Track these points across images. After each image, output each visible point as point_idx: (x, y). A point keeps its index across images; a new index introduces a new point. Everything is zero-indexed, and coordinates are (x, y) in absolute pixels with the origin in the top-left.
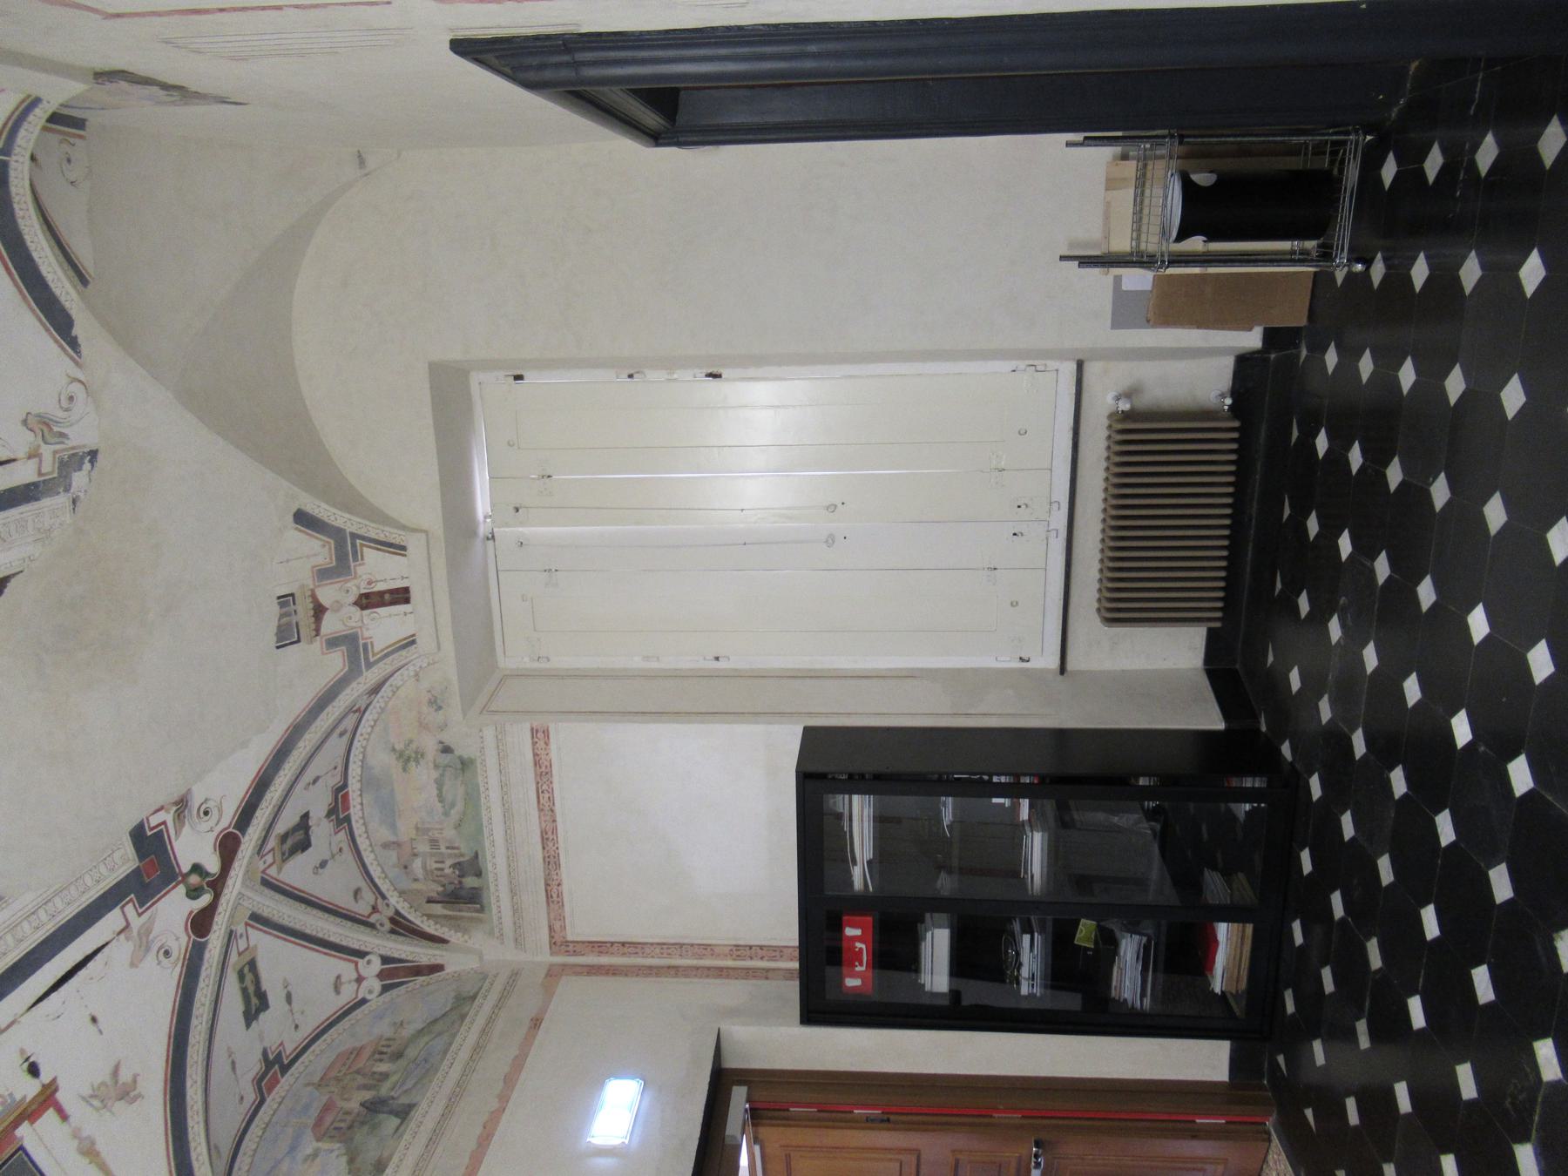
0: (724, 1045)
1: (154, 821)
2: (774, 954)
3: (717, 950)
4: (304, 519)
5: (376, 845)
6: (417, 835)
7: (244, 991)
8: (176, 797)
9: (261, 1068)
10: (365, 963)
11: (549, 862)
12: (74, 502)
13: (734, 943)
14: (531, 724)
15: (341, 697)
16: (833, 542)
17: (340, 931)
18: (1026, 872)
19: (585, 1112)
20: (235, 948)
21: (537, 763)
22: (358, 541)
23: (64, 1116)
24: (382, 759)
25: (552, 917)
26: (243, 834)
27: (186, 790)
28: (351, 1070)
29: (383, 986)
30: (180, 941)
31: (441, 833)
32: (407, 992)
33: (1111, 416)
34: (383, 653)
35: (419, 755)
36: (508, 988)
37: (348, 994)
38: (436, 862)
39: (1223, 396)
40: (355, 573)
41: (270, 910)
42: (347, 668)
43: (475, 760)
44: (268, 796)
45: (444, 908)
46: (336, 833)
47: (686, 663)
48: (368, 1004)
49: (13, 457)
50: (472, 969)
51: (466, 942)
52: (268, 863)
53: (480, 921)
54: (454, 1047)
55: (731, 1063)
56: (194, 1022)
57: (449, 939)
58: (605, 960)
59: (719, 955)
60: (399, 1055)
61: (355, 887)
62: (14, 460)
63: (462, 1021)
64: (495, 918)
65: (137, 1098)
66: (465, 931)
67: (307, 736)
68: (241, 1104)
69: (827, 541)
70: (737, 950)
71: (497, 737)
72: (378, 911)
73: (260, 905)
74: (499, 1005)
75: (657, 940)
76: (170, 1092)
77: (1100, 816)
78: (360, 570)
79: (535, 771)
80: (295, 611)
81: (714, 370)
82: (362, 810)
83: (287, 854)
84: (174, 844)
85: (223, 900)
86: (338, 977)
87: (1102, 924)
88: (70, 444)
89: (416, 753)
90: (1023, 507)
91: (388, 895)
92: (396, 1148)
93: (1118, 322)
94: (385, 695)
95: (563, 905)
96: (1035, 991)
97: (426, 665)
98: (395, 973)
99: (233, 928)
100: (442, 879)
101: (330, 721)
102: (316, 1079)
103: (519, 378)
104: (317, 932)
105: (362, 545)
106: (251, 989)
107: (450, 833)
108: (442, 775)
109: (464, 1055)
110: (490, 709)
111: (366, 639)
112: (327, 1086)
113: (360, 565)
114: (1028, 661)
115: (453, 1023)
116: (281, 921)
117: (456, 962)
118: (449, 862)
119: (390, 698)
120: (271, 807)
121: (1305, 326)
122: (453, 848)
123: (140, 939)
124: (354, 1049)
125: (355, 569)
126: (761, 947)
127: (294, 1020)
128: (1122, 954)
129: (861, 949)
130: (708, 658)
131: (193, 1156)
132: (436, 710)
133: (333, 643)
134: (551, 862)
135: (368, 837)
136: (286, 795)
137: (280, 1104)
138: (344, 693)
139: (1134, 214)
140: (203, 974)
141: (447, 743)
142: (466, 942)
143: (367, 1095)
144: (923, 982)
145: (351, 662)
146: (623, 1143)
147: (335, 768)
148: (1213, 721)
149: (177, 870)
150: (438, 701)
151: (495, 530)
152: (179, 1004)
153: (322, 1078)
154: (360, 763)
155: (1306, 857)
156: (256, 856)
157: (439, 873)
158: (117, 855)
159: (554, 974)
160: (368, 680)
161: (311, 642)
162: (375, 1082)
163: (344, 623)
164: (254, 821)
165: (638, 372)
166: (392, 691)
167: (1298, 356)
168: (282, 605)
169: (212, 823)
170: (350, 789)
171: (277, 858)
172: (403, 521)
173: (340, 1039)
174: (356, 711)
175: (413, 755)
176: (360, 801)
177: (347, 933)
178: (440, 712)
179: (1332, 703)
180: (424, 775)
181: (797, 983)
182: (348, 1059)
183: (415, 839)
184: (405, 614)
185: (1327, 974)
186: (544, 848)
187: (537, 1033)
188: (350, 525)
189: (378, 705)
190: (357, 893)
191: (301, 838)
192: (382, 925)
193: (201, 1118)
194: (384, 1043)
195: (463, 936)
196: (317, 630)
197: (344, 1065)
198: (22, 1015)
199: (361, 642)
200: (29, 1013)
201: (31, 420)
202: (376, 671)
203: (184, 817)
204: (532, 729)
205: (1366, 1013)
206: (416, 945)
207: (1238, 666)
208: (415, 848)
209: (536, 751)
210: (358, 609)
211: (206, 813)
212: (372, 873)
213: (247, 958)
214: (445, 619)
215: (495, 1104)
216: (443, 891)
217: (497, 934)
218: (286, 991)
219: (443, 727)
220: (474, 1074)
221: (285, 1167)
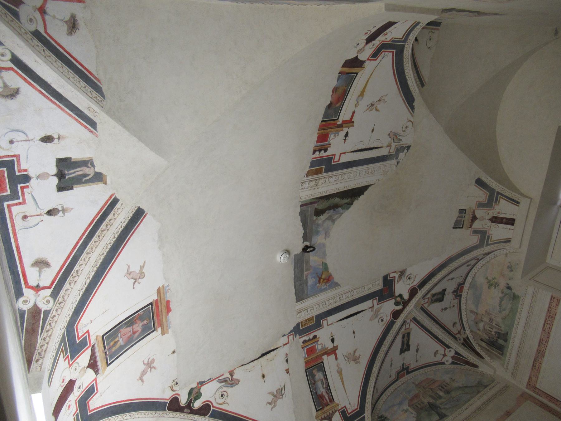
1: (392, 275)
4: (480, 183)
7: (403, 342)
8: (401, 270)
12: (398, 163)
15: (472, 253)
20: (404, 326)
21: (549, 311)
22: (499, 196)
23: (336, 359)
24: (481, 280)
26: (420, 290)
27: (405, 268)
30: (387, 318)
32: (461, 369)
35: (496, 285)
37: (439, 358)
38: (489, 327)
40: (494, 207)
42: (478, 242)
44: (433, 279)
46: (454, 299)
49: (382, 146)
51: (491, 362)
52: (425, 302)
54: (470, 402)
56: (383, 346)
57: (484, 358)
62: (382, 147)
63: (477, 394)
65: (358, 363)
66: (492, 358)
67: (454, 263)
68: (390, 378)
71: (534, 292)
72: (460, 334)
74: (495, 396)
76: (368, 365)
78: (496, 207)
79: (547, 314)
80: (464, 216)
82: (467, 295)
83: (433, 301)
84: (396, 285)
85: (405, 310)
86: (437, 351)
88: (402, 143)
89: (496, 283)
94: (491, 257)
97: (512, 252)
99: (406, 320)
100: (490, 335)
101: (465, 260)
102: (417, 383)
105: (500, 197)
106: (406, 342)
107: (499, 319)
108: (504, 297)
111: (489, 234)
118: (494, 330)
123: (375, 313)
124: (434, 380)
127: (417, 358)
133: (476, 232)
134: (540, 353)
135: (466, 305)
136: (439, 281)
140: (391, 332)
141: (510, 285)
143: (432, 401)
147: (462, 276)
149: (394, 294)
150: (512, 268)
152: (380, 338)
156: (422, 298)
157: (489, 332)
158: (377, 283)
159: (524, 397)
160: (485, 250)
161: (467, 229)
166: (494, 256)
168: (460, 213)
169: (410, 282)
170: (465, 285)
172: (522, 191)
180: (496, 294)
182: (430, 382)
183: (484, 315)
184: (510, 229)
186: (539, 346)
188: (498, 188)
191: (439, 297)
192: (460, 340)
193: (375, 379)
194: (445, 384)
196: (471, 226)
198: (335, 322)
199: (487, 235)
200: (337, 323)
201: (391, 135)
203: (402, 277)
204: (552, 296)
211: (409, 278)
213: (407, 331)
214: (527, 237)
218: (417, 348)
219: (511, 279)
221: (395, 408)
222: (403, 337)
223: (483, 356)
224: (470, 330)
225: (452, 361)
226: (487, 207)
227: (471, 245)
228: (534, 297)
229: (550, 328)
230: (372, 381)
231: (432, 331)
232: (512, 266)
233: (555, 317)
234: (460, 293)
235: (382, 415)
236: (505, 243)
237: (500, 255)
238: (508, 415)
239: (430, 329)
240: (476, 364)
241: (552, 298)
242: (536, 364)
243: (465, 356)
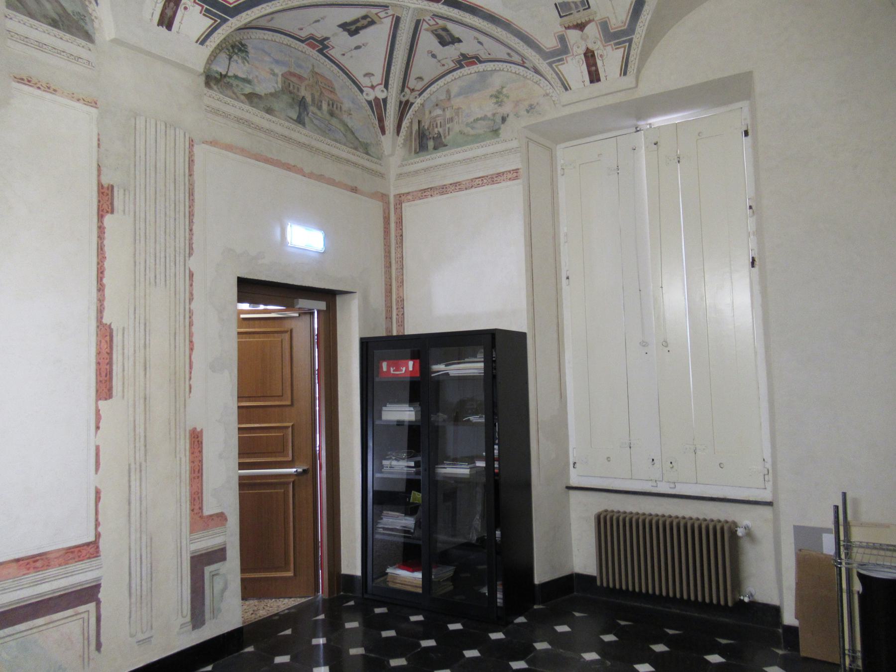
0: (348, 296)
2: (400, 321)
3: (401, 289)
6: (455, 109)
7: (357, 21)
9: (319, 38)
13: (405, 298)
14: (521, 168)
15: (530, 50)
16: (644, 346)
17: (397, 73)
18: (448, 464)
19: (305, 221)
21: (498, 175)
24: (496, 81)
28: (322, 89)
29: (371, 101)
33: (735, 524)
34: (558, 71)
35: (500, 103)
36: (373, 172)
37: (364, 82)
38: (441, 122)
39: (751, 595)
40: (608, 45)
41: (403, 28)
44: (467, 15)
46: (452, 61)
47: (564, 260)
48: (360, 94)
50: (384, 151)
52: (429, 22)
54: (338, 145)
55: (339, 300)
58: (393, 225)
59: (398, 290)
60: (332, 114)
61: (424, 78)
64: (412, 161)
66: (404, 145)
69: (643, 342)
70: (401, 301)
71: (513, 149)
72: (411, 92)
73: (405, 21)
74: (364, 168)
75: (404, 254)
77: (479, 508)
80: (579, 11)
81: (757, 263)
82: (468, 74)
83: (436, 33)
87: (420, 508)
90: (671, 466)
92: (280, 119)
93: (799, 531)
95: (420, 199)
96: (385, 468)
97: (553, 99)
98: (378, 106)
99: (390, 8)
100: (432, 127)
102: (316, 70)
103: (746, 133)
104: (395, 59)
106: (359, 24)
108: (489, 119)
109: (335, 151)
110: (529, 143)
111: (566, 59)
112: (313, 77)
113: (612, 48)
114: (574, 467)
115: (352, 143)
116: (398, 35)
117: (387, 141)
118: (441, 130)
119: (532, 81)
120: (461, 18)
121: (799, 654)
122: (449, 132)
124: (334, 89)
125: (609, 45)
126: (403, 314)
128: (406, 518)
129: (402, 370)
130: (568, 272)
131: (264, 6)
132: (527, 110)
133: (562, 39)
134: (443, 190)
135: (452, 80)
137: (302, 52)
138: (532, 51)
139: (881, 544)
141: (508, 119)
143: (309, 99)
144: (387, 406)
145: (550, 52)
146: (289, 243)
147: (489, 54)
148: (540, 577)
151: (643, 131)
153: (317, 73)
154: (494, 69)
155: (458, 626)
156: (432, 14)
157: (435, 125)
159: (383, 197)
162: (316, 103)
163: (574, 44)
164: (451, 9)
165: (753, 212)
166: (537, 81)
167: (779, 647)
171: (433, 27)
173: (339, 81)
174: (523, 62)
176: (472, 72)
177: (396, 76)
178: (525, 113)
179: (546, 651)
180: (489, 108)
181: (384, 335)
182: (329, 86)
184: (584, 82)
185: (391, 633)
186: (451, 184)
187: (348, 191)
189: (528, 74)
190: (420, 78)
192: (404, 96)
195: (401, 144)
196: (569, 28)
197: (325, 84)
199: (564, 57)
202: (547, 69)
204: (518, 169)
205: (368, 654)
207: (575, 593)
208: (448, 110)
209: (505, 173)
210: (584, 52)
212: (433, 86)
213: (376, 19)
215: (307, 170)
216: (425, 129)
217: (404, 163)
218: (361, 45)
219: (517, 115)
220: (324, 158)
221: (267, 59)
222: (365, 17)
223: (400, 134)
226: (604, 36)
227: (541, 44)
228: (507, 152)
229: (479, 186)
230: (280, 4)
233: (494, 184)
234: (465, 63)
235: (246, 45)
238: (353, 191)
240: (386, 130)
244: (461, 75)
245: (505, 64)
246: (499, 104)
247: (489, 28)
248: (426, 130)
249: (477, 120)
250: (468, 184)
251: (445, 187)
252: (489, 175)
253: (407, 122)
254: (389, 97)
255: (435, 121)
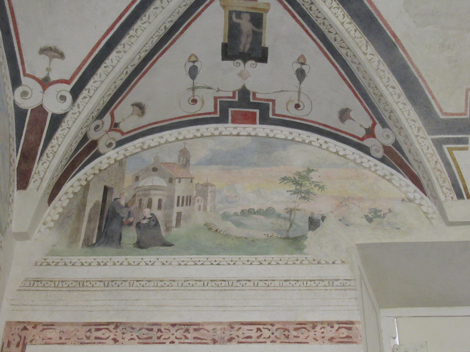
5: (185, 143)
10: (63, 93)
11: (151, 330)
14: (359, 322)
15: (409, 106)
21: (301, 325)
25: (65, 328)
31: (199, 209)
38: (160, 201)
42: (442, 117)
43: (302, 253)
45: (96, 204)
50: (11, 222)
53: (73, 240)
61: (147, 110)
64: (75, 259)
71: (336, 280)
82: (231, 135)
86: (62, 56)
89: (308, 192)
91: (121, 149)
95: (82, 343)
97: (425, 210)
100: (137, 204)
108: (279, 216)
118: (159, 214)
141: (323, 225)
142: (44, 224)
145: (447, 122)
150: (378, 219)
157: (145, 202)
160: (421, 140)
175: (303, 189)
178: (364, 221)
183: (191, 182)
186: (174, 325)
204: (352, 323)
206: (57, 169)
208: (180, 182)
209: (319, 326)
216: (119, 203)
217: (50, 259)
223: (54, 202)
224: (122, 159)
225: (26, 111)
227: (433, 98)
228: (322, 284)
229: (249, 340)
231: (136, 27)
232: (384, 217)
236: (453, 185)
237: (397, 187)
239: (145, 19)
240: (32, 181)
241: (346, 323)
242: (108, 329)
243: (50, 145)
244: (199, 135)
245: (314, 137)
246: (303, 195)
247: (354, 38)
248: (121, 207)
249: (251, 212)
250: (219, 333)
251: (155, 328)
252: (279, 323)
253: (77, 183)
254: (68, 118)
255: (147, 195)
